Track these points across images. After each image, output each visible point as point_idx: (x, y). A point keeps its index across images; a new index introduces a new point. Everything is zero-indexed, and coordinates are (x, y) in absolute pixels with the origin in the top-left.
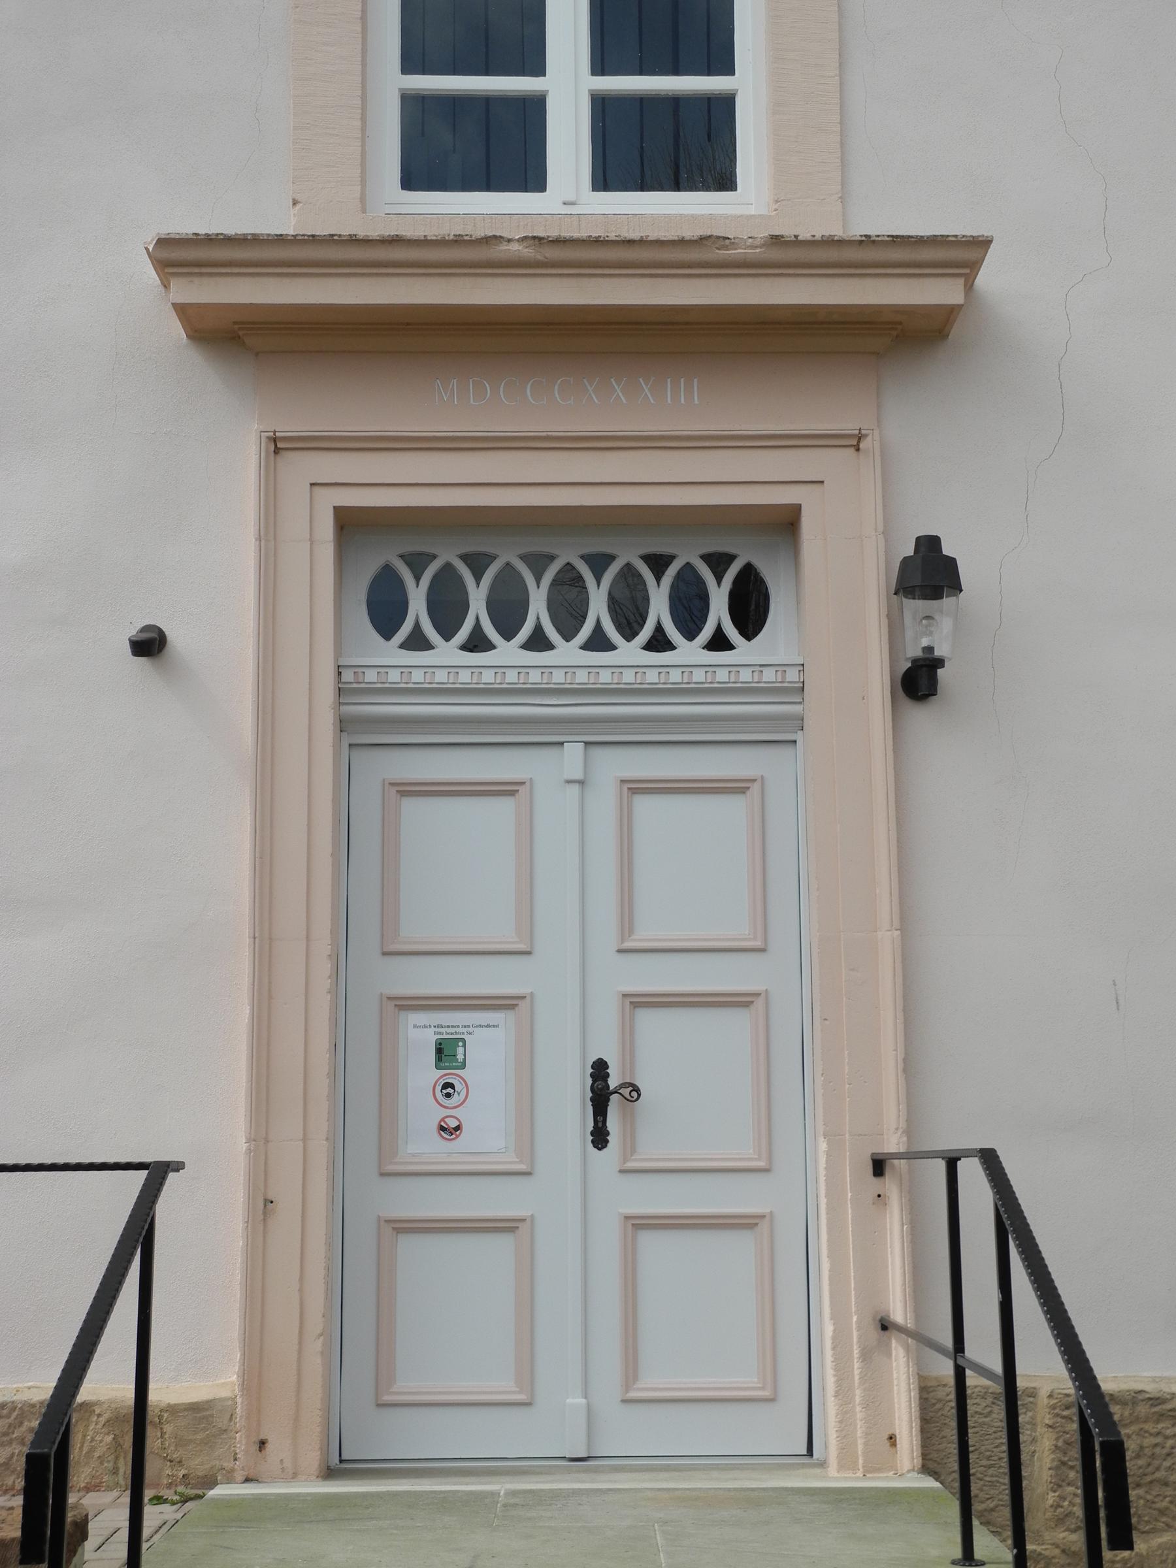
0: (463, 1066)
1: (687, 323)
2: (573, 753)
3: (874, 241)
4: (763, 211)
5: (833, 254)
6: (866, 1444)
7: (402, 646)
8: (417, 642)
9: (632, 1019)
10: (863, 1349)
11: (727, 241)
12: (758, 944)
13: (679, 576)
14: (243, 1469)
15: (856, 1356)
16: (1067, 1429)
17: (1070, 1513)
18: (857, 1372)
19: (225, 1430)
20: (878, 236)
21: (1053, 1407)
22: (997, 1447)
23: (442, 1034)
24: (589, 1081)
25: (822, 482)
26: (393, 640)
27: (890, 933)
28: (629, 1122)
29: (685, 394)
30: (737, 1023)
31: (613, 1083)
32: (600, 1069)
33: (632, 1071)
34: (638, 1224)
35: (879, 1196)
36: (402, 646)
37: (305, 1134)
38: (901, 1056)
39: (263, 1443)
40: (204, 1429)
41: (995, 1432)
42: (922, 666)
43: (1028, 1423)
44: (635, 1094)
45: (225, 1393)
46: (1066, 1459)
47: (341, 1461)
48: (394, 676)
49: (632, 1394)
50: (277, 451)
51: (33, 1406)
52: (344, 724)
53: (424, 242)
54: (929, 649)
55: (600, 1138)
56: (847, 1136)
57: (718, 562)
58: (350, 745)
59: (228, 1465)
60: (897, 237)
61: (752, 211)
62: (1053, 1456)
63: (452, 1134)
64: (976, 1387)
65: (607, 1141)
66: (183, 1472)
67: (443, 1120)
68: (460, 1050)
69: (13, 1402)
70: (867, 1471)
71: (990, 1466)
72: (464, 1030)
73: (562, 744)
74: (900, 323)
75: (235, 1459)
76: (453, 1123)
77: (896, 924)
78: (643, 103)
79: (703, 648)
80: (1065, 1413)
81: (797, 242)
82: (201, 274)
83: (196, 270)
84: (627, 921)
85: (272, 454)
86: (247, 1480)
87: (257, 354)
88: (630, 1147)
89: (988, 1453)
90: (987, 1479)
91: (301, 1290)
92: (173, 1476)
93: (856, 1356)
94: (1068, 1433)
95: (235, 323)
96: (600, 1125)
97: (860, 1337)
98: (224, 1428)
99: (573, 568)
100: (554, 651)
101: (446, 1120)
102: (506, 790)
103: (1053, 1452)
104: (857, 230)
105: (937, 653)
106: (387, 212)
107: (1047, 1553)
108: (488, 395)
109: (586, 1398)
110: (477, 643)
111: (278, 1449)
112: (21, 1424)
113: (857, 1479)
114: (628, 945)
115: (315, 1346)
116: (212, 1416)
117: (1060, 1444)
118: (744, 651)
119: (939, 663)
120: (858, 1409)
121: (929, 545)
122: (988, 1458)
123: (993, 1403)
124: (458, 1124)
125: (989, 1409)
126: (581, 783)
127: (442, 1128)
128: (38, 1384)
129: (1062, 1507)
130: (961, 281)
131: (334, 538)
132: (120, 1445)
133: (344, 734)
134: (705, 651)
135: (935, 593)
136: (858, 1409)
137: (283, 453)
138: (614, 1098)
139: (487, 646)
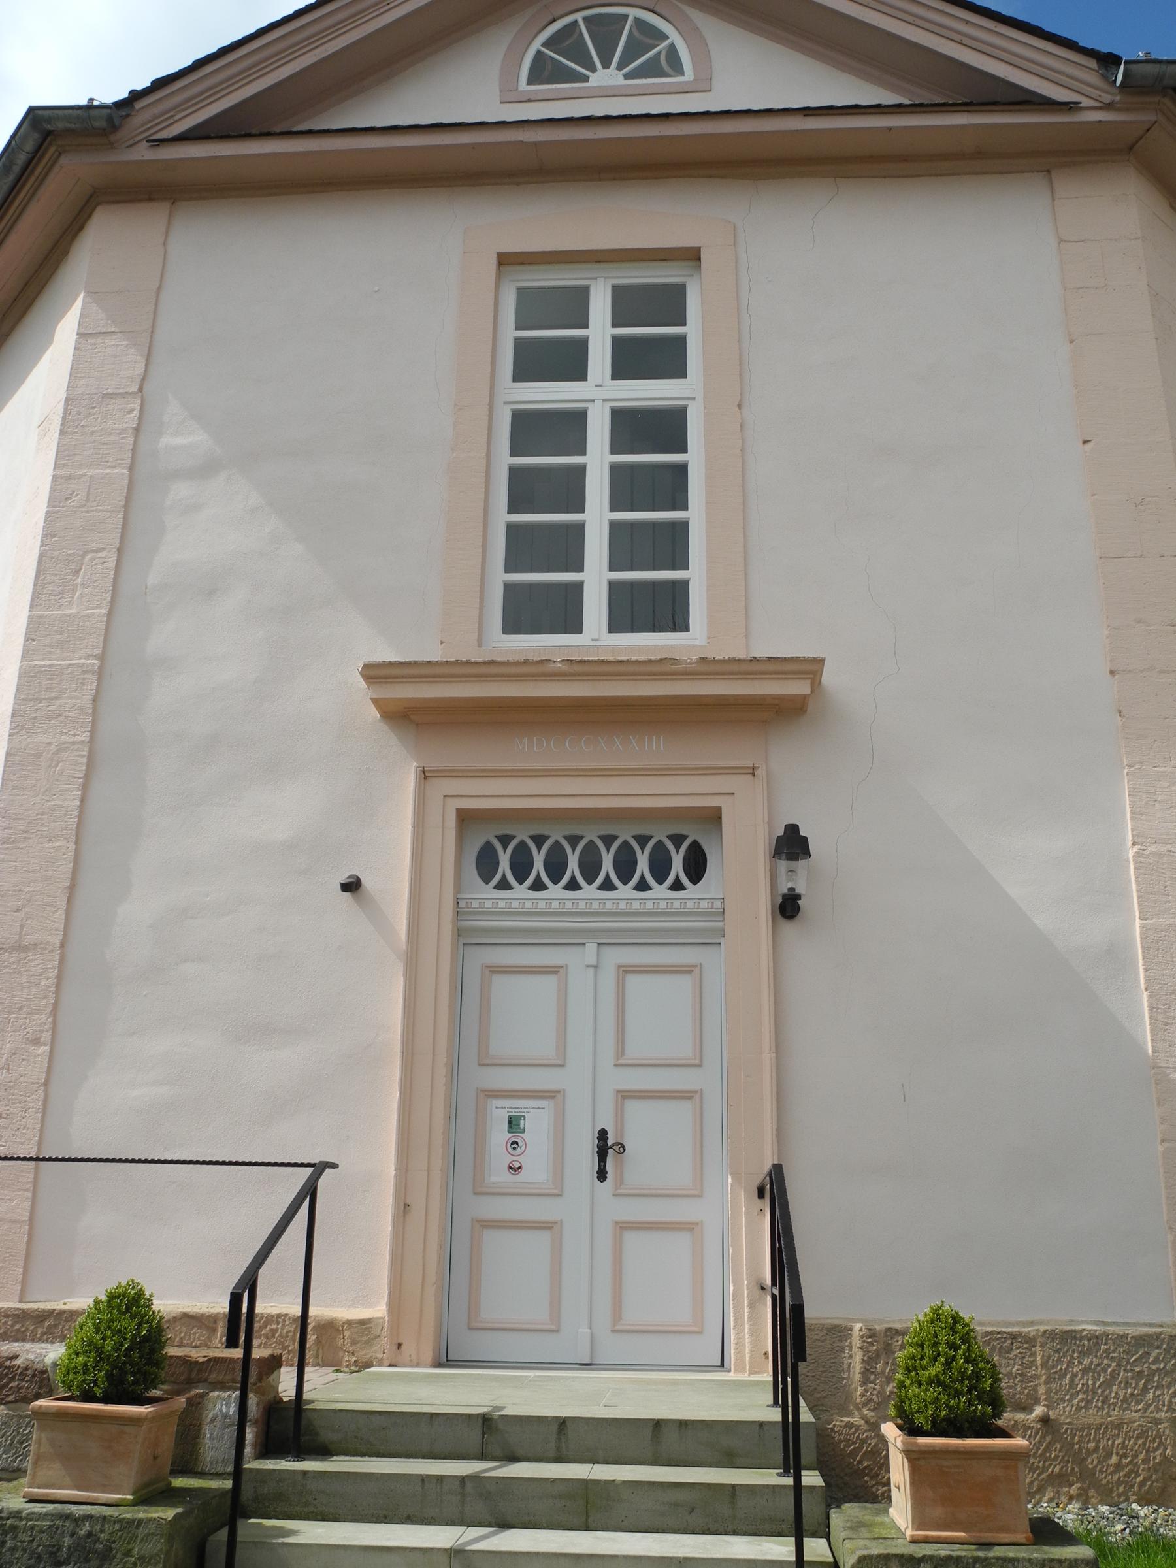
0: (524, 1131)
1: (656, 706)
2: (591, 948)
3: (758, 660)
4: (704, 643)
5: (735, 668)
6: (751, 1357)
7: (495, 888)
8: (504, 885)
9: (622, 1105)
10: (751, 1301)
11: (676, 661)
12: (697, 1062)
13: (620, 848)
14: (388, 1359)
15: (746, 1305)
16: (870, 1350)
17: (871, 1399)
18: (746, 1314)
19: (379, 1336)
20: (760, 657)
21: (862, 1337)
22: (828, 1360)
23: (512, 1112)
24: (597, 1141)
25: (733, 794)
26: (490, 884)
27: (769, 1055)
28: (620, 1166)
29: (663, 744)
30: (684, 1109)
31: (610, 1142)
32: (603, 1134)
33: (622, 1136)
34: (623, 1227)
35: (761, 1210)
36: (495, 888)
37: (428, 1167)
38: (775, 1127)
39: (400, 1345)
40: (367, 1335)
41: (827, 1351)
42: (788, 899)
43: (847, 1346)
44: (622, 1149)
45: (379, 1315)
46: (869, 1367)
47: (447, 1360)
48: (488, 904)
49: (618, 1327)
50: (426, 778)
51: (273, 1316)
52: (459, 932)
53: (507, 663)
54: (792, 889)
55: (602, 1175)
56: (743, 1175)
57: (678, 840)
58: (464, 944)
59: (380, 1356)
60: (771, 658)
61: (698, 643)
62: (861, 1365)
63: (516, 1171)
64: (816, 1324)
65: (606, 1177)
66: (355, 1359)
67: (511, 1163)
68: (522, 1122)
69: (262, 1314)
70: (751, 1373)
71: (825, 1371)
72: (525, 1110)
73: (584, 944)
74: (777, 705)
75: (384, 1353)
76: (517, 1165)
77: (773, 1049)
78: (632, 584)
79: (668, 889)
80: (870, 1340)
81: (714, 661)
82: (386, 683)
83: (383, 680)
84: (620, 1049)
85: (423, 779)
86: (390, 1366)
87: (417, 724)
88: (620, 1182)
89: (823, 1364)
90: (823, 1379)
91: (424, 1257)
92: (349, 1361)
93: (746, 1305)
94: (870, 1352)
95: (405, 708)
96: (602, 1167)
97: (748, 1294)
98: (378, 1335)
99: (560, 843)
100: (582, 891)
101: (513, 1163)
102: (552, 970)
103: (862, 1363)
104: (761, 652)
105: (798, 891)
106: (494, 646)
107: (856, 1423)
108: (545, 745)
109: (590, 1329)
110: (538, 886)
111: (409, 1349)
112: (266, 1326)
113: (746, 1377)
114: (621, 1061)
115: (431, 1291)
116: (371, 1328)
117: (865, 1358)
118: (692, 891)
119: (798, 897)
120: (747, 1336)
121: (792, 829)
122: (824, 1367)
123: (827, 1334)
124: (520, 1165)
125: (824, 1338)
126: (596, 967)
127: (510, 1168)
128: (277, 1305)
129: (866, 1396)
130: (809, 682)
131: (456, 825)
132: (320, 1342)
133: (461, 938)
134: (669, 891)
135: (793, 857)
136: (747, 1336)
137: (429, 779)
138: (610, 1151)
139: (543, 887)
